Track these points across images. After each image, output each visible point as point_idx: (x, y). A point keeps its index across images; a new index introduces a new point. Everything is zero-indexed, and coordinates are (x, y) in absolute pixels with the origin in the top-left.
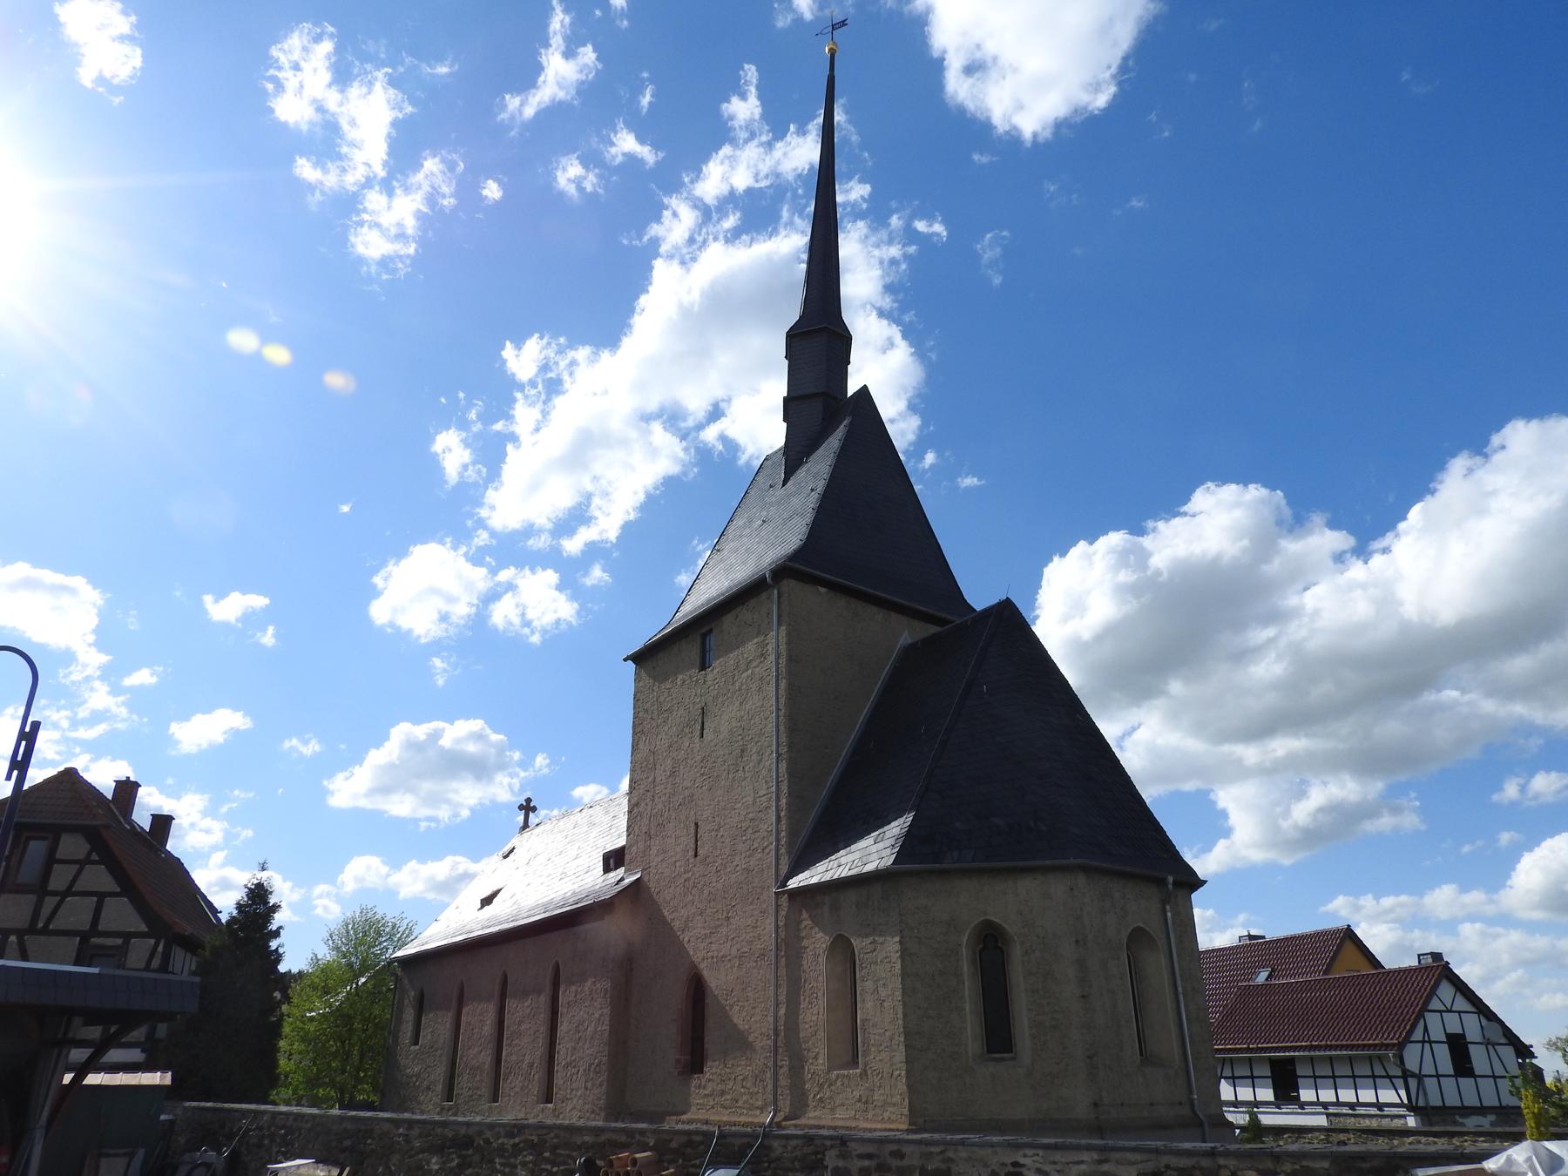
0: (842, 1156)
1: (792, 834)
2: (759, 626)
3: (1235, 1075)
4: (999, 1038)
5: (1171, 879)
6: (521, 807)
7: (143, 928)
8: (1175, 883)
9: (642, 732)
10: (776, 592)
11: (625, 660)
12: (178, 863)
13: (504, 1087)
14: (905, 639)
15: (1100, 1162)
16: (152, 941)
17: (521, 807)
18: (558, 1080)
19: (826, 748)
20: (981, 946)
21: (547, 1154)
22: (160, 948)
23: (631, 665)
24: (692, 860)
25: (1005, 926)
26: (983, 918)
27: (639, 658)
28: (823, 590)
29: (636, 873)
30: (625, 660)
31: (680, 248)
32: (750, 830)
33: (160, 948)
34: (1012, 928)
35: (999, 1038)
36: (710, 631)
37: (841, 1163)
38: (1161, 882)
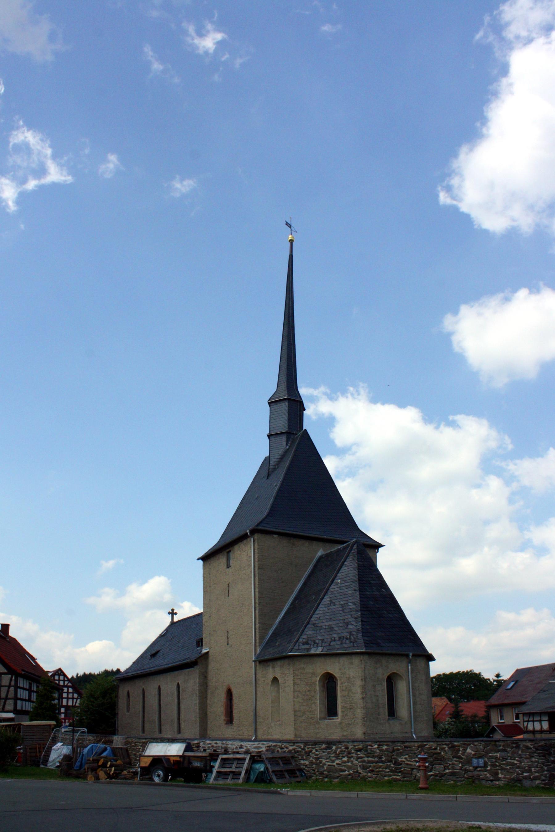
0: (204, 744)
1: (262, 638)
2: (248, 552)
3: (542, 719)
4: (332, 711)
5: (411, 654)
6: (169, 613)
7: (5, 671)
8: (413, 656)
9: (207, 591)
10: (252, 539)
11: (198, 559)
12: (14, 640)
13: (163, 728)
14: (320, 553)
15: (258, 744)
16: (10, 676)
17: (169, 613)
18: (182, 726)
19: (278, 603)
20: (327, 681)
21: (133, 744)
22: (13, 678)
23: (201, 562)
24: (227, 646)
25: (334, 674)
26: (326, 671)
27: (205, 558)
28: (275, 536)
29: (206, 649)
30: (198, 559)
31: (59, 689)
32: (246, 636)
33: (13, 678)
34: (337, 674)
35: (332, 711)
36: (230, 551)
37: (204, 746)
38: (407, 656)
